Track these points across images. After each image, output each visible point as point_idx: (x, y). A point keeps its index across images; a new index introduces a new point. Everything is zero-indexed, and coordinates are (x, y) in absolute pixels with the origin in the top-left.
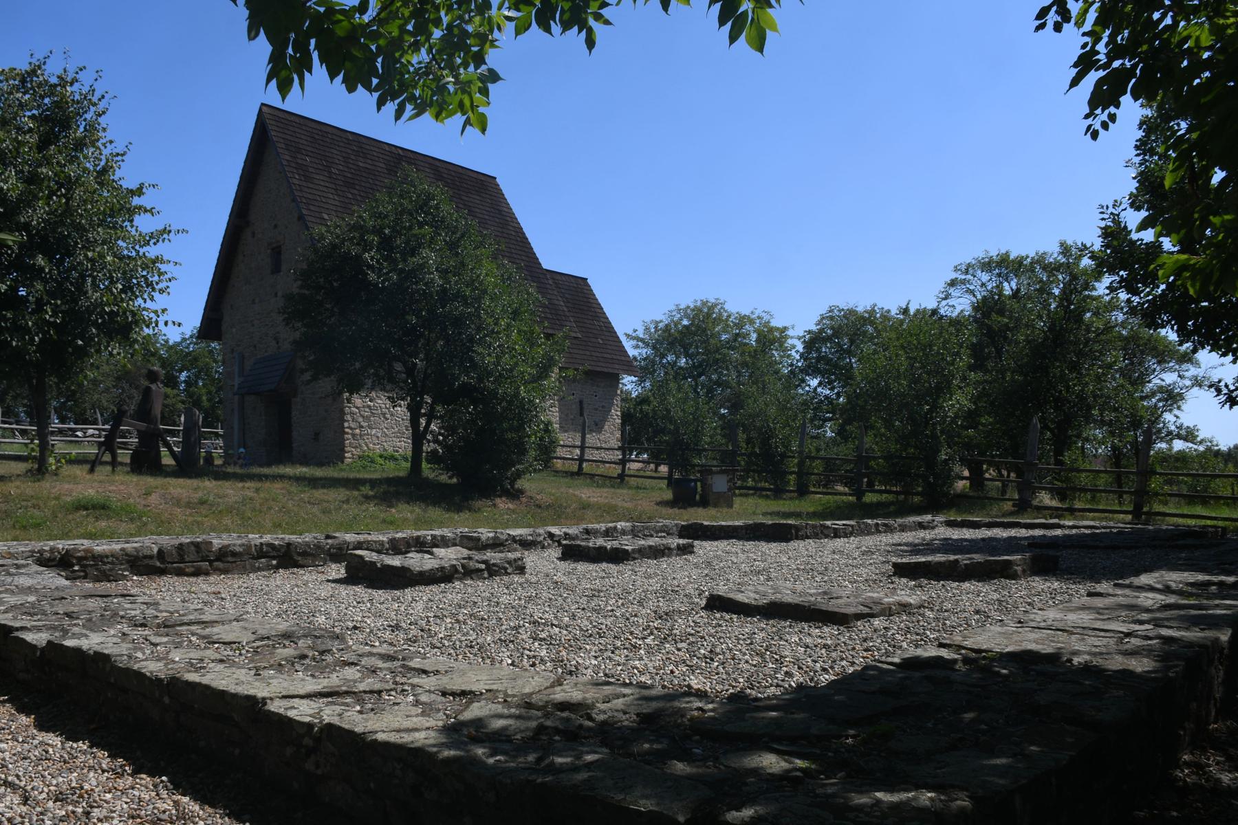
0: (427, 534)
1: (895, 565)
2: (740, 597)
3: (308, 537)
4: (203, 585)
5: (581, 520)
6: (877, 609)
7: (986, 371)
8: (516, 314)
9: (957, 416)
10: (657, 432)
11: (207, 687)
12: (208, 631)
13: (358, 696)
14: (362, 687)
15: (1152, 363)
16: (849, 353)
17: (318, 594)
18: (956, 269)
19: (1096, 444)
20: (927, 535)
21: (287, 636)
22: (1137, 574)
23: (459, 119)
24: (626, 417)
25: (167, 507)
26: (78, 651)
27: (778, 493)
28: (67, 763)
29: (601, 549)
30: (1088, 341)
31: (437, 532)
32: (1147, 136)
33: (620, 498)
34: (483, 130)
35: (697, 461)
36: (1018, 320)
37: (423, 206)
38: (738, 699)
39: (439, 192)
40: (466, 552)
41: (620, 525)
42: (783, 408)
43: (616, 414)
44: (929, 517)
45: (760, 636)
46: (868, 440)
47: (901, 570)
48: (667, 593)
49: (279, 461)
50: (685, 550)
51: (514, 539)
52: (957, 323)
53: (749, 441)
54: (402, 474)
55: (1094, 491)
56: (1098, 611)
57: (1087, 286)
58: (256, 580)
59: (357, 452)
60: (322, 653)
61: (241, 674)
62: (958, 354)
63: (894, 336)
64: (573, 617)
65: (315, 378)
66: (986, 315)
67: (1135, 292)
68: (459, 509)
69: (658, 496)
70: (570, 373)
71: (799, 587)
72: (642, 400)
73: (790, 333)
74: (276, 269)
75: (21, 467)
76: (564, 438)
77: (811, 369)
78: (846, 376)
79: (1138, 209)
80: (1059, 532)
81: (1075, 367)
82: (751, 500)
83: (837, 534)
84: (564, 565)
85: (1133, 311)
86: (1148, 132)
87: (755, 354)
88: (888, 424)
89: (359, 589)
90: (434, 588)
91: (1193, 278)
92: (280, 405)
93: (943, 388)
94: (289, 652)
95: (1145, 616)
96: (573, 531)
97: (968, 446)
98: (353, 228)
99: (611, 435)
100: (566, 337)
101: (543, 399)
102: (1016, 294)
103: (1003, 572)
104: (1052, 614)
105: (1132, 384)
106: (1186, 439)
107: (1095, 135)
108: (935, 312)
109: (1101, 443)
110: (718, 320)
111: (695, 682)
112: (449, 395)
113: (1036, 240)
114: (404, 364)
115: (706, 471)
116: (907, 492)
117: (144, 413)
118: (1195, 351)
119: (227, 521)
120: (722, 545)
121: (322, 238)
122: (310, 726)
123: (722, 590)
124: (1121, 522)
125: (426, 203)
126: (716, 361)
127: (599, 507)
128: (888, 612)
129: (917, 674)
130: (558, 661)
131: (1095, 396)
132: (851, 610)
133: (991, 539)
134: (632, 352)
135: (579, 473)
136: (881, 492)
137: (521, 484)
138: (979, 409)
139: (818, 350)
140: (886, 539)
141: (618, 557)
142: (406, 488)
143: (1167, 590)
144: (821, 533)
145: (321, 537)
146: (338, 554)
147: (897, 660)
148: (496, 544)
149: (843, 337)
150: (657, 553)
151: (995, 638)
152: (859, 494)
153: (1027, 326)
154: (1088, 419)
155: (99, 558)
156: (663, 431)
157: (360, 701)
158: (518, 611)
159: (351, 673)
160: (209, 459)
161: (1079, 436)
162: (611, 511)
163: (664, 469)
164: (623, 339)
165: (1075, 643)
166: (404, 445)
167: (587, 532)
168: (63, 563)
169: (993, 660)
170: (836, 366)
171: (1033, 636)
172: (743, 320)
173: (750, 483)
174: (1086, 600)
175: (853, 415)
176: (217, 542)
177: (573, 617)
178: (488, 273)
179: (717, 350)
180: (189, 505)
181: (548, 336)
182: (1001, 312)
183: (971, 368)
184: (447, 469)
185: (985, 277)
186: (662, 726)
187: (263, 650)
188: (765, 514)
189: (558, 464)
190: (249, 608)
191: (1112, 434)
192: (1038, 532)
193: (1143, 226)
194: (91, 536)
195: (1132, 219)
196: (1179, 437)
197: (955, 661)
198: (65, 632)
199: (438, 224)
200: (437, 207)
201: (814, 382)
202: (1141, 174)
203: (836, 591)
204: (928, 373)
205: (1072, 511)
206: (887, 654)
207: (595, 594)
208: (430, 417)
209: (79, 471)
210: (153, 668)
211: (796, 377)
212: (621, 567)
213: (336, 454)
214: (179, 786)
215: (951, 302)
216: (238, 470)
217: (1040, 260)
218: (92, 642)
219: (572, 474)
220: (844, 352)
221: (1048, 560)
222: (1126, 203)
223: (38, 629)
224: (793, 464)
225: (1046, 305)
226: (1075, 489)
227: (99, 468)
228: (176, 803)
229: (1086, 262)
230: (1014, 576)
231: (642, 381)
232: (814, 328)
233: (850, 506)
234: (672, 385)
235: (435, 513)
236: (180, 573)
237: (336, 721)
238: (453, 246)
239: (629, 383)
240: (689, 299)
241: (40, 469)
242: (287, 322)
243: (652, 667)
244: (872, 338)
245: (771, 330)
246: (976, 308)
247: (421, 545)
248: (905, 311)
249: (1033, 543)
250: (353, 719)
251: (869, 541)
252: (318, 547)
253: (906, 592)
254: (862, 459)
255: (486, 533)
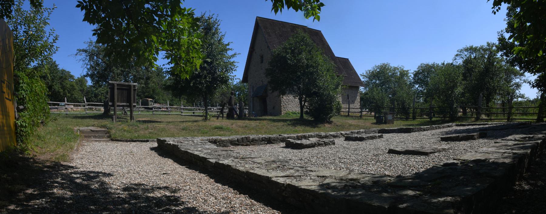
0: (307, 134)
1: (441, 138)
2: (397, 149)
3: (274, 136)
4: (249, 148)
5: (349, 129)
6: (436, 150)
7: (467, 81)
8: (328, 70)
9: (459, 94)
10: (371, 103)
11: (256, 174)
12: (253, 160)
13: (295, 177)
14: (296, 175)
15: (513, 76)
16: (427, 77)
17: (278, 151)
18: (458, 51)
19: (498, 100)
20: (450, 129)
21: (274, 161)
22: (508, 136)
23: (312, 18)
24: (362, 99)
25: (237, 128)
26: (223, 164)
27: (407, 119)
28: (223, 191)
29: (356, 137)
30: (495, 70)
31: (309, 134)
32: (509, 12)
33: (361, 122)
34: (319, 20)
35: (383, 111)
36: (476, 65)
37: (302, 40)
38: (399, 177)
39: (306, 35)
40: (318, 139)
41: (361, 130)
42: (408, 94)
43: (358, 98)
44: (451, 124)
45: (404, 160)
46: (433, 102)
47: (443, 139)
48: (377, 149)
49: (264, 115)
50: (381, 137)
51: (331, 135)
52: (458, 67)
53: (398, 104)
54: (298, 118)
55: (497, 114)
56: (497, 147)
57: (495, 55)
58: (262, 147)
59: (285, 112)
60: (283, 166)
61: (264, 171)
62: (459, 76)
63: (440, 71)
64: (350, 156)
65: (273, 92)
66: (467, 64)
67: (508, 56)
68: (314, 127)
69: (372, 121)
70: (345, 87)
71: (414, 146)
72: (366, 94)
73: (409, 72)
74: (262, 62)
75: (200, 118)
76: (343, 106)
77: (416, 82)
78: (426, 84)
79: (508, 33)
80: (487, 126)
81: (492, 78)
82: (399, 121)
83: (424, 130)
84: (345, 142)
85: (507, 62)
86: (510, 11)
87: (399, 79)
88: (439, 97)
89: (289, 149)
90: (310, 149)
91: (523, 54)
92: (263, 100)
93: (455, 86)
94: (275, 165)
95: (509, 148)
96: (348, 132)
97: (462, 103)
98: (283, 48)
99: (357, 104)
100: (343, 76)
101: (337, 95)
102: (475, 58)
103: (472, 138)
104: (485, 149)
105: (508, 83)
106: (522, 98)
107: (495, 13)
108: (452, 64)
109: (499, 100)
110: (388, 69)
111: (387, 173)
112: (310, 95)
113: (480, 42)
114: (297, 86)
115: (386, 114)
116: (444, 117)
117: (230, 103)
118: (524, 73)
119: (252, 131)
120: (391, 135)
121: (275, 52)
122: (283, 184)
123: (392, 148)
124: (504, 122)
125: (303, 39)
126: (388, 81)
127: (354, 125)
128: (439, 151)
129: (447, 167)
130: (347, 168)
131: (497, 87)
132: (429, 151)
133: (468, 129)
134: (362, 80)
135: (348, 115)
136: (437, 117)
137: (332, 119)
138: (461, 93)
139: (418, 77)
140: (438, 131)
141: (361, 139)
142: (300, 122)
143: (515, 140)
144: (420, 130)
145: (278, 135)
146: (283, 140)
147: (442, 164)
148: (326, 137)
149: (425, 73)
150: (372, 138)
151: (469, 156)
152: (431, 118)
153: (478, 67)
154: (495, 93)
155: (223, 141)
156: (373, 102)
157: (296, 178)
158: (334, 155)
159: (292, 171)
160: (245, 115)
161: (493, 98)
162: (359, 127)
163: (373, 114)
164: (360, 76)
165: (490, 156)
166: (298, 110)
167: (352, 132)
168: (214, 142)
169: (468, 162)
170: (423, 81)
171: (479, 155)
172: (395, 69)
173: (399, 116)
174: (494, 144)
175: (429, 95)
176: (251, 137)
177: (350, 156)
178: (320, 59)
179: (388, 78)
180: (243, 127)
181: (338, 76)
182: (471, 63)
183: (463, 80)
184: (311, 116)
185: (466, 53)
186: (378, 185)
187: (268, 164)
188: (403, 125)
189: (342, 113)
190: (261, 154)
191: (502, 97)
192: (481, 126)
193: (510, 38)
194: (220, 135)
195: (507, 36)
196: (520, 97)
197: (458, 163)
198: (219, 160)
199: (307, 45)
200: (306, 40)
201: (417, 86)
202: (508, 23)
203: (425, 146)
204: (451, 82)
205: (491, 120)
206: (439, 162)
207: (356, 150)
208: (305, 101)
209: (215, 119)
210: (241, 169)
211: (411, 85)
212: (362, 142)
213: (279, 113)
214: (251, 197)
215: (456, 61)
216: (254, 118)
217: (481, 48)
218: (226, 162)
219: (346, 116)
220: (426, 77)
221: (484, 134)
222: (505, 31)
223: (213, 159)
224: (411, 111)
225: (484, 61)
226: (492, 113)
227: (220, 118)
228: (251, 201)
229: (494, 48)
230: (475, 139)
231: (366, 88)
232: (417, 70)
233: (428, 122)
234: (375, 89)
235: (308, 128)
236: (242, 145)
237: (290, 183)
238: (310, 52)
239: (362, 89)
240: (379, 63)
241: (206, 119)
242: (266, 76)
243: (375, 169)
244: (434, 72)
245: (404, 71)
246: (464, 62)
247: (305, 137)
248: (443, 64)
249: (480, 129)
250: (294, 183)
251: (434, 132)
252: (277, 138)
253: (445, 145)
254: (431, 108)
255: (323, 134)
